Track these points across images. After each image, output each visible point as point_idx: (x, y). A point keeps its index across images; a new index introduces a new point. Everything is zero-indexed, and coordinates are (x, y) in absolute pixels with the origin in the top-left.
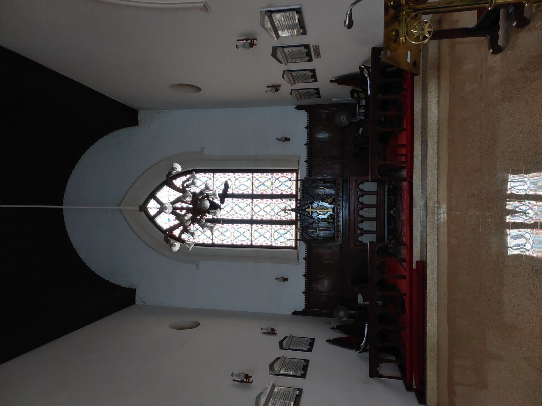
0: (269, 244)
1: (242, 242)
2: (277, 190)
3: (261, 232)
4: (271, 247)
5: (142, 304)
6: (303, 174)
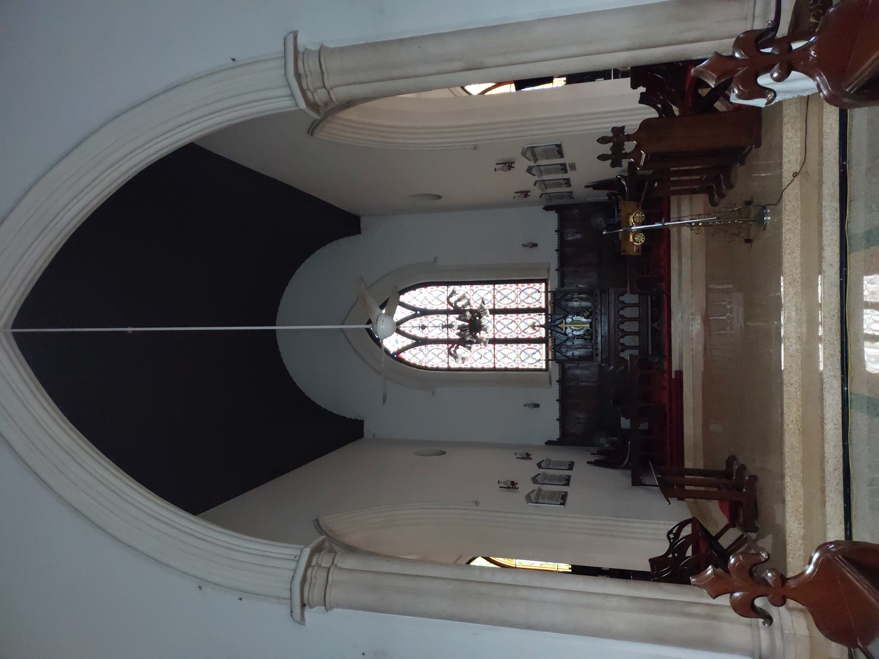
2: (523, 304)
4: (517, 370)
6: (554, 284)
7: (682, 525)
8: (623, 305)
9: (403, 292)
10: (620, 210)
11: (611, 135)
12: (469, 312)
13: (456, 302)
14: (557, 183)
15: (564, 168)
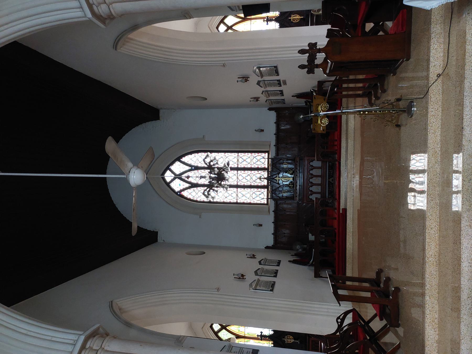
0: (249, 202)
1: (230, 200)
2: (255, 165)
3: (243, 194)
4: (250, 204)
5: (163, 242)
6: (273, 154)
7: (346, 313)
8: (312, 168)
9: (184, 155)
10: (312, 111)
11: (308, 48)
12: (216, 169)
13: (210, 163)
14: (274, 93)
15: (279, 83)
